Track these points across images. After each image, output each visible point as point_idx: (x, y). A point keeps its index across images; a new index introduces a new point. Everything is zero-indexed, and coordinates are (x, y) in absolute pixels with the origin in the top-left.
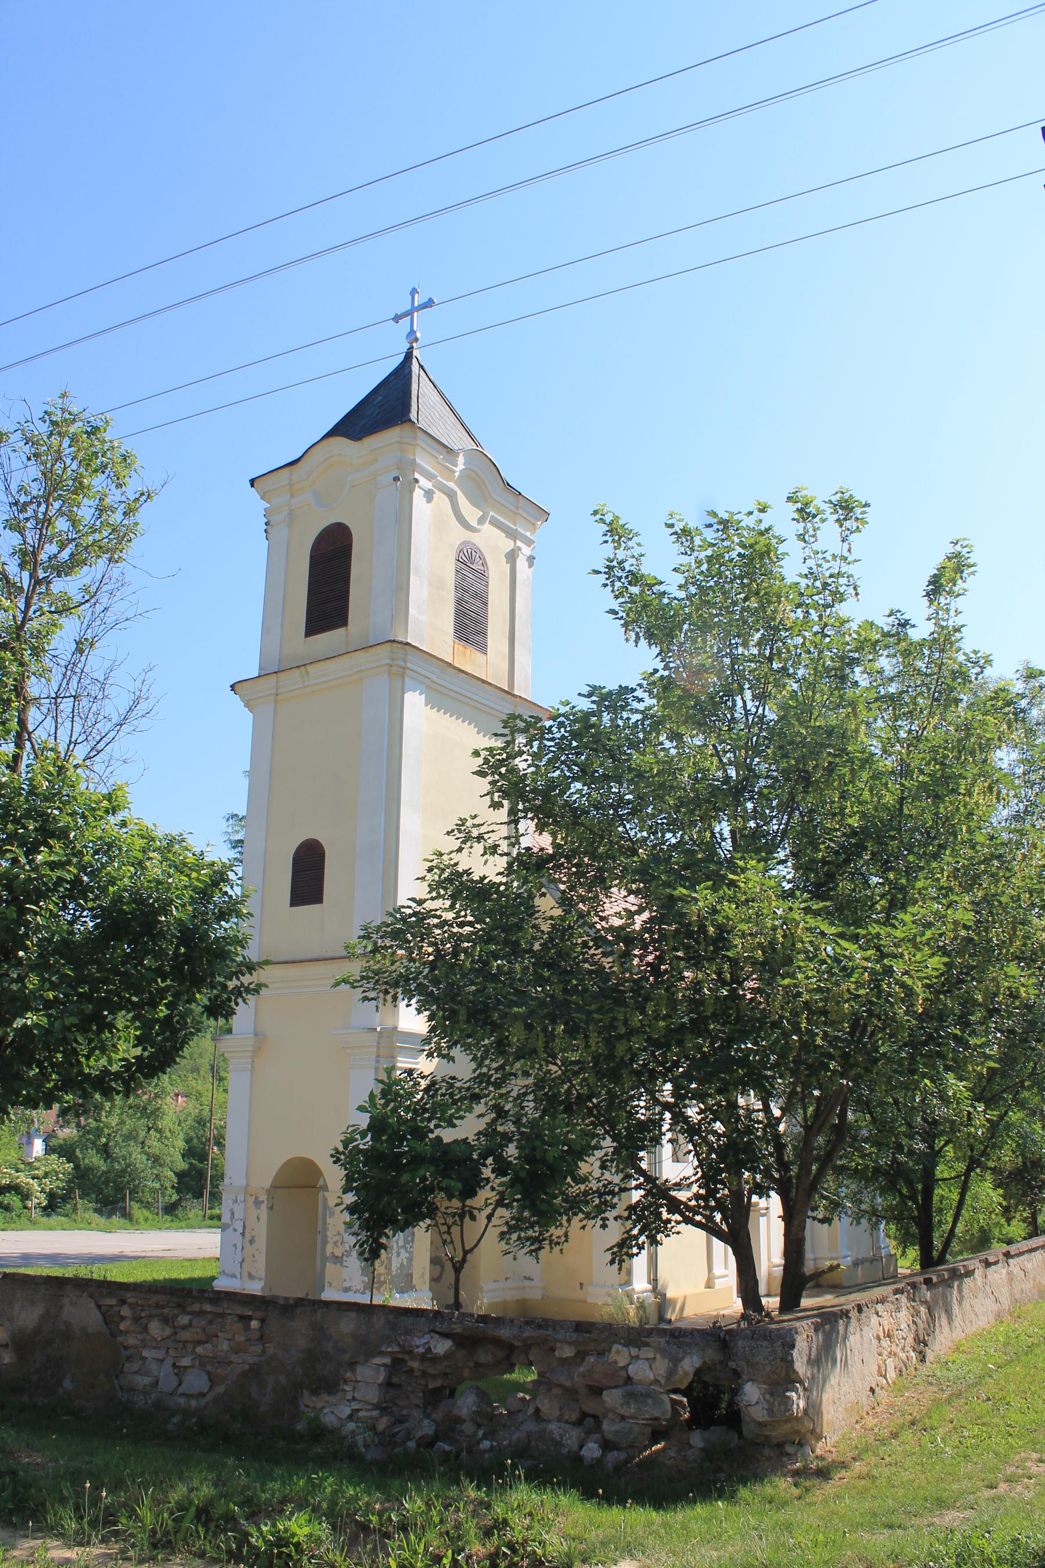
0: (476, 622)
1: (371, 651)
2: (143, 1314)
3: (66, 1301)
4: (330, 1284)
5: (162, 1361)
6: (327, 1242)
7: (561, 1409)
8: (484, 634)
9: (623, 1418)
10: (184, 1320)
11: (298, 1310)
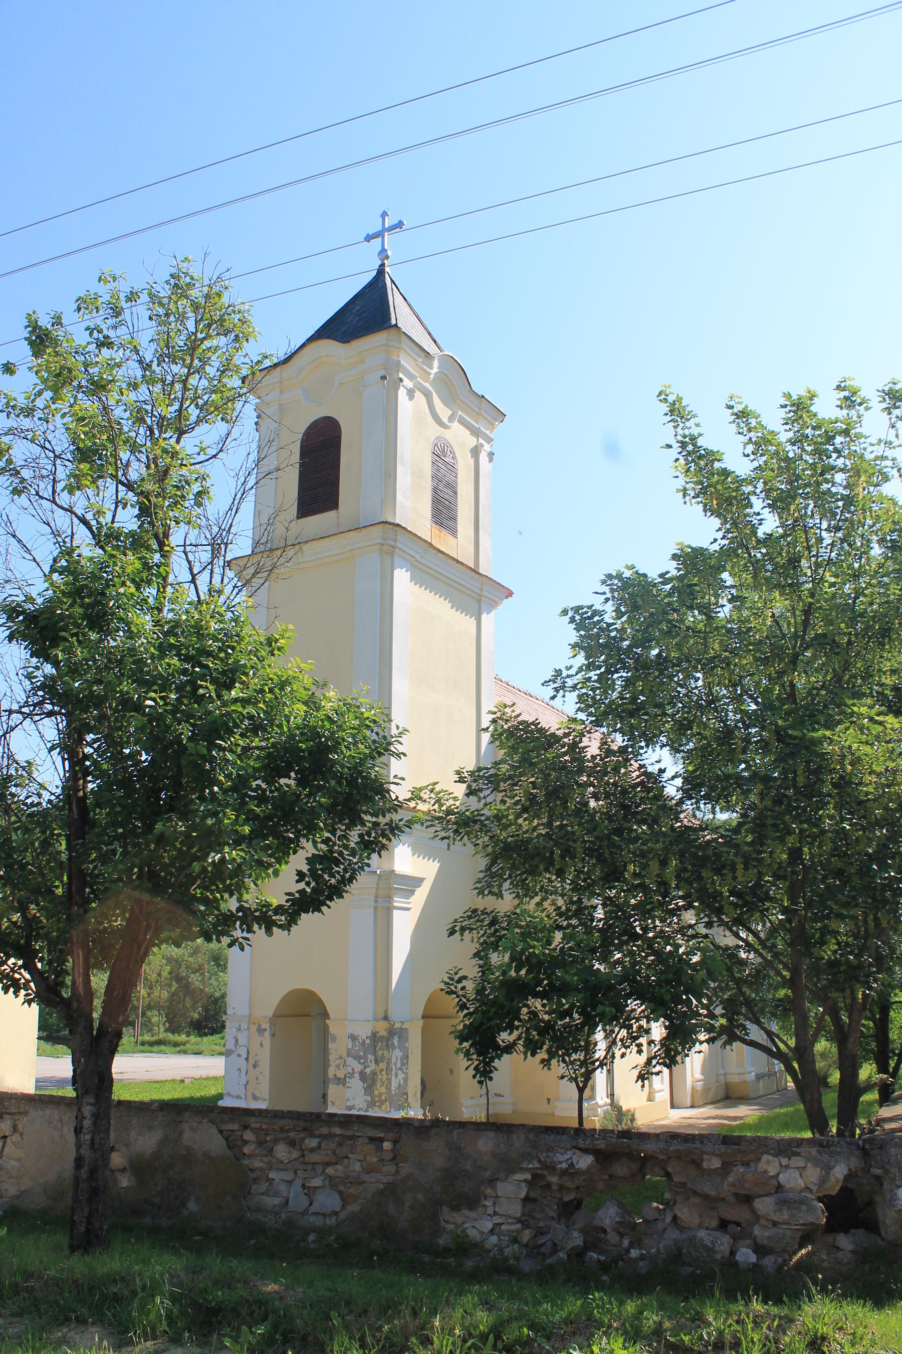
0: (449, 508)
1: (364, 530)
2: (268, 1138)
3: (186, 1127)
4: (333, 1103)
5: (290, 1182)
6: (329, 1066)
7: (700, 1216)
8: (454, 519)
9: (775, 1224)
10: (312, 1143)
11: (433, 1132)
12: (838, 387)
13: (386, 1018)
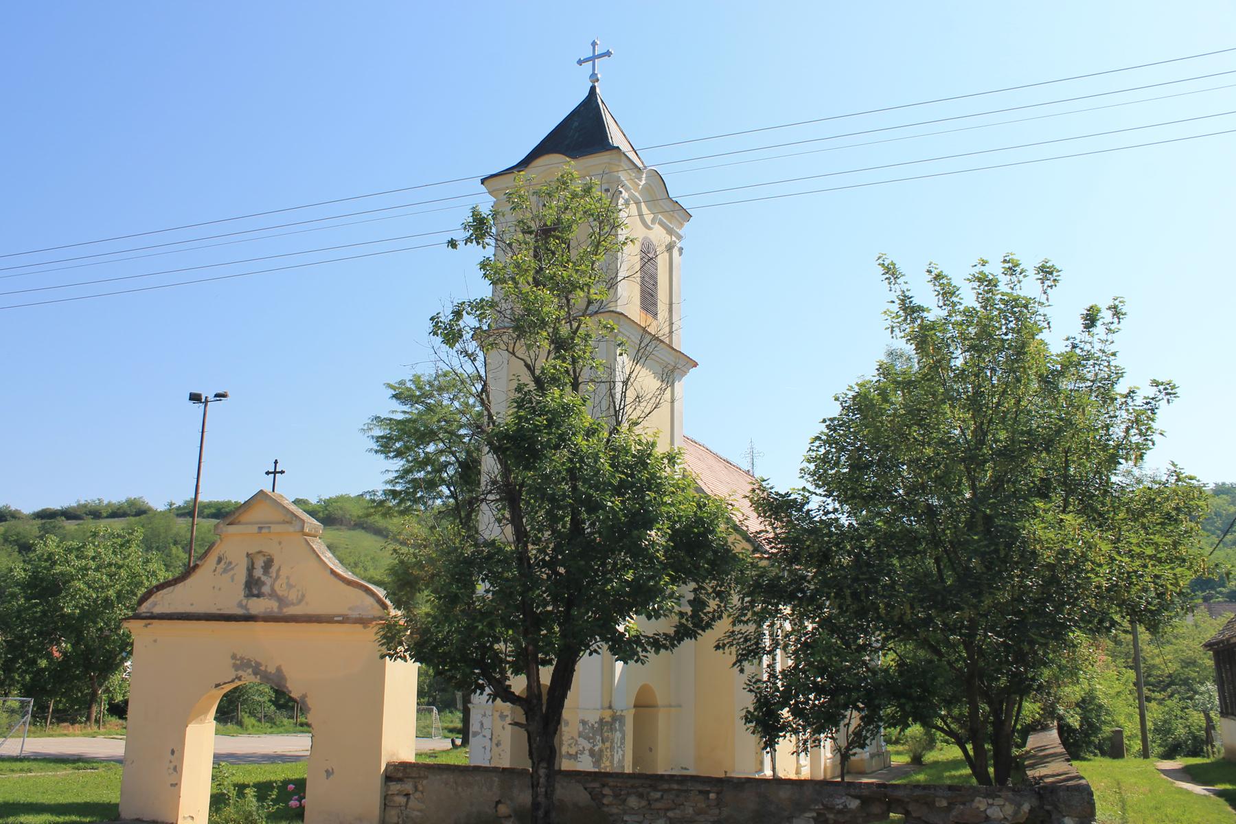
8: (655, 304)
12: (1005, 261)
13: (610, 707)
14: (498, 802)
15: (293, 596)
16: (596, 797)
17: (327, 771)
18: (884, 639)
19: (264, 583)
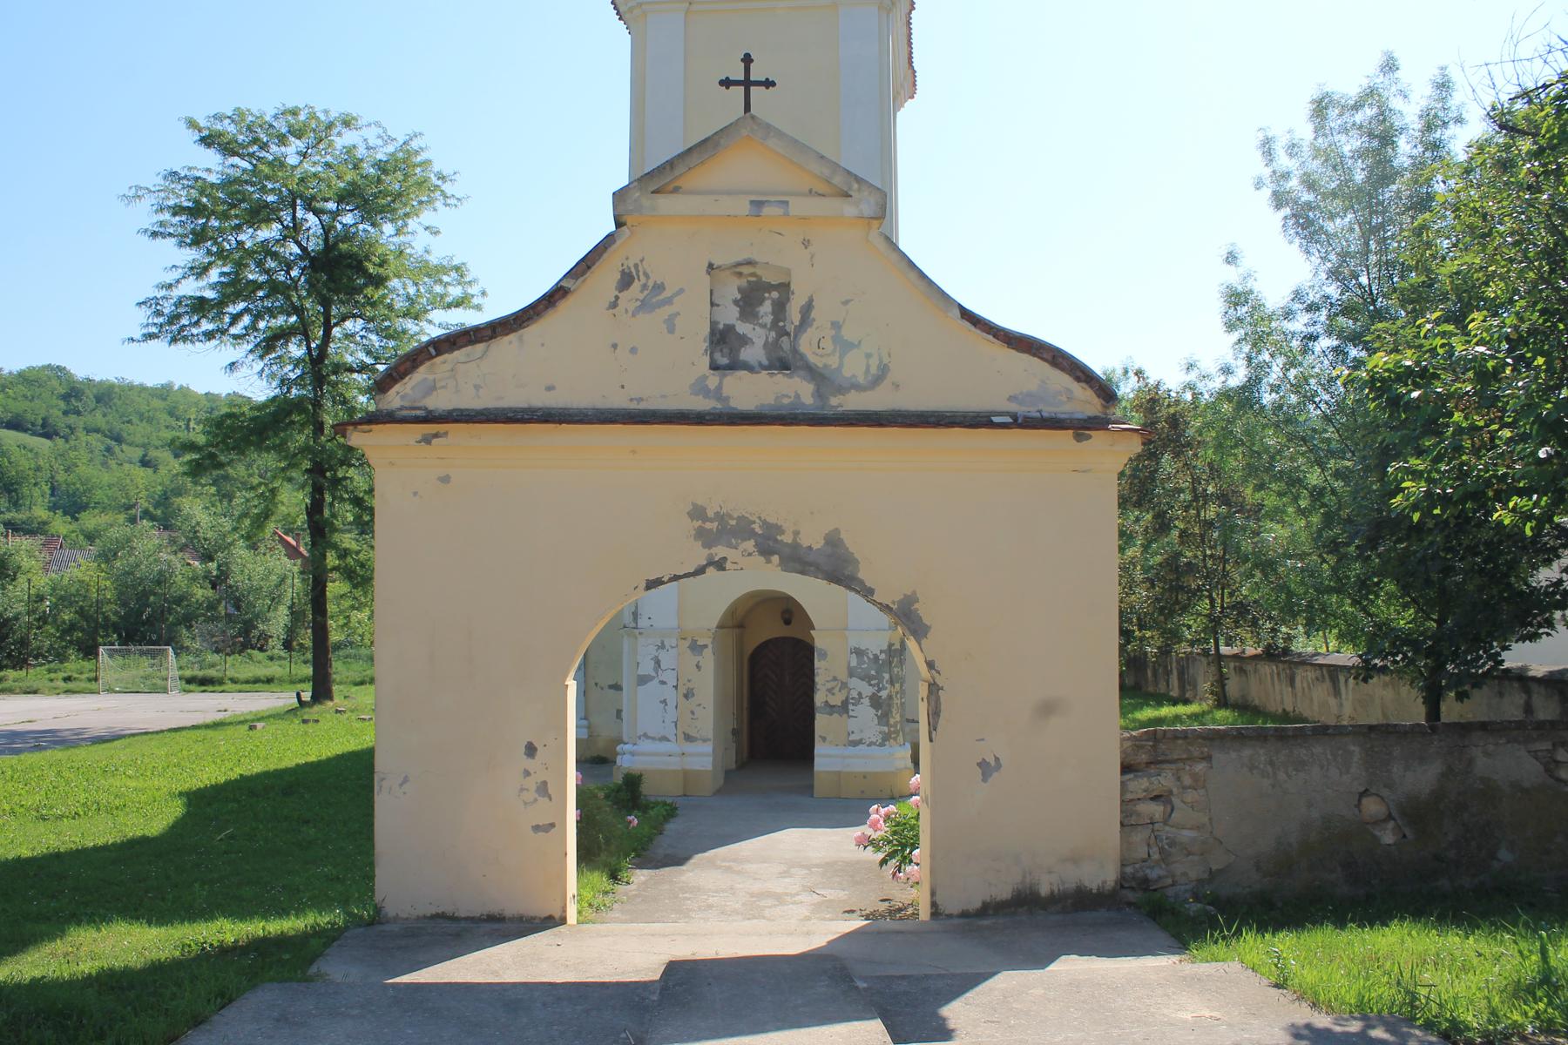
4: (824, 739)
14: (1363, 794)
15: (854, 367)
16: (1551, 766)
17: (983, 765)
18: (96, 621)
19: (744, 340)
